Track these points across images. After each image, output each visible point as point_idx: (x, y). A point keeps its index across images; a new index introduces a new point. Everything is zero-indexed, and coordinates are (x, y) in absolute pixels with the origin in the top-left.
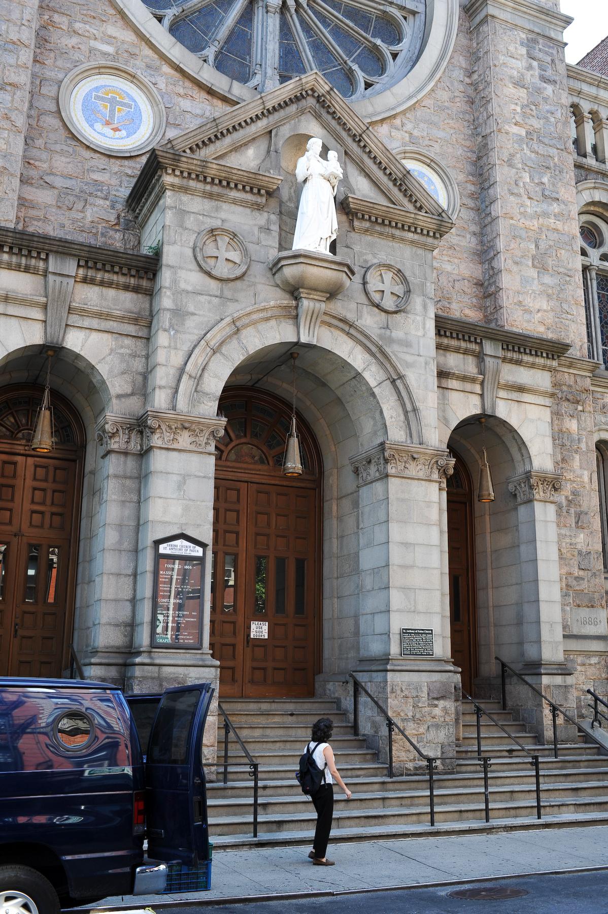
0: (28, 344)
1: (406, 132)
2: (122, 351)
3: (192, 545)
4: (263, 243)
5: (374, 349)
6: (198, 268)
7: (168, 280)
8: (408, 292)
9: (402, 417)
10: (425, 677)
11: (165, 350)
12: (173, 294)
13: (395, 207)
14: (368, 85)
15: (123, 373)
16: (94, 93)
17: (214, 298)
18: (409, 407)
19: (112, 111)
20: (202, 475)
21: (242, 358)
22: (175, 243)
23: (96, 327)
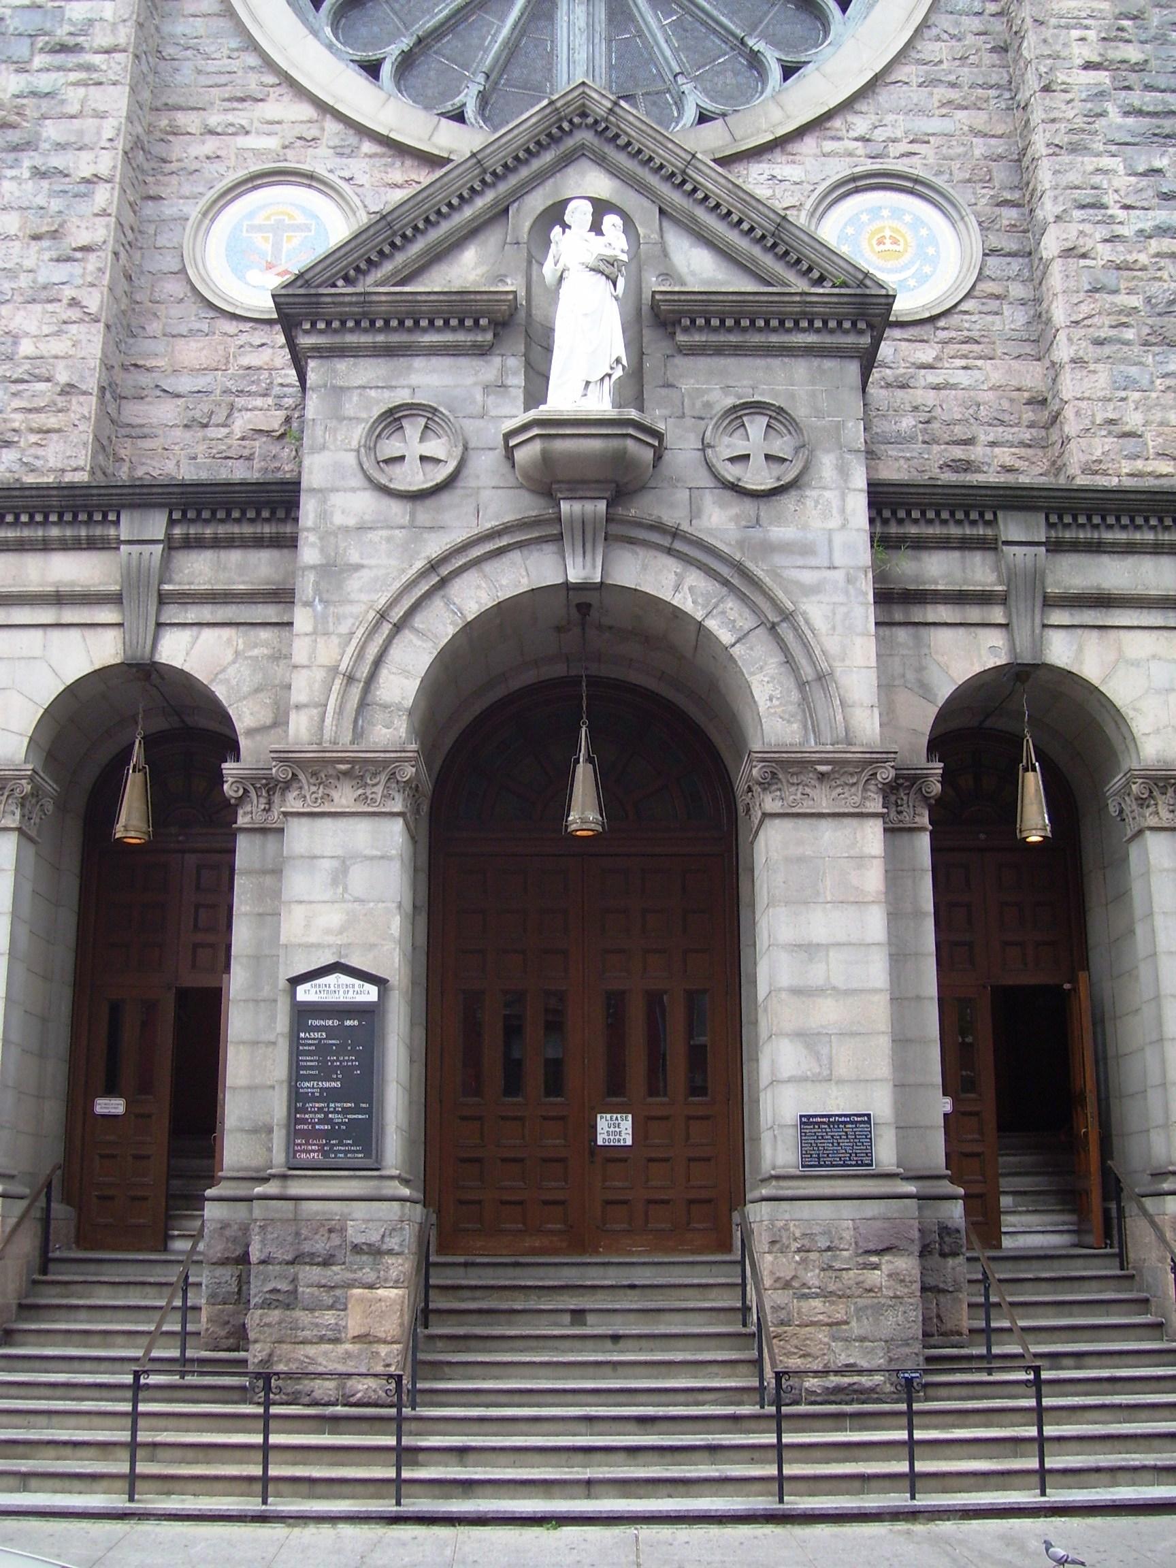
0: (97, 667)
1: (856, 139)
3: (357, 982)
4: (493, 413)
5: (725, 571)
6: (366, 484)
7: (311, 516)
10: (848, 1210)
11: (307, 639)
12: (321, 539)
13: (771, 289)
14: (789, 71)
17: (397, 532)
19: (277, 247)
20: (379, 853)
21: (451, 631)
22: (324, 447)
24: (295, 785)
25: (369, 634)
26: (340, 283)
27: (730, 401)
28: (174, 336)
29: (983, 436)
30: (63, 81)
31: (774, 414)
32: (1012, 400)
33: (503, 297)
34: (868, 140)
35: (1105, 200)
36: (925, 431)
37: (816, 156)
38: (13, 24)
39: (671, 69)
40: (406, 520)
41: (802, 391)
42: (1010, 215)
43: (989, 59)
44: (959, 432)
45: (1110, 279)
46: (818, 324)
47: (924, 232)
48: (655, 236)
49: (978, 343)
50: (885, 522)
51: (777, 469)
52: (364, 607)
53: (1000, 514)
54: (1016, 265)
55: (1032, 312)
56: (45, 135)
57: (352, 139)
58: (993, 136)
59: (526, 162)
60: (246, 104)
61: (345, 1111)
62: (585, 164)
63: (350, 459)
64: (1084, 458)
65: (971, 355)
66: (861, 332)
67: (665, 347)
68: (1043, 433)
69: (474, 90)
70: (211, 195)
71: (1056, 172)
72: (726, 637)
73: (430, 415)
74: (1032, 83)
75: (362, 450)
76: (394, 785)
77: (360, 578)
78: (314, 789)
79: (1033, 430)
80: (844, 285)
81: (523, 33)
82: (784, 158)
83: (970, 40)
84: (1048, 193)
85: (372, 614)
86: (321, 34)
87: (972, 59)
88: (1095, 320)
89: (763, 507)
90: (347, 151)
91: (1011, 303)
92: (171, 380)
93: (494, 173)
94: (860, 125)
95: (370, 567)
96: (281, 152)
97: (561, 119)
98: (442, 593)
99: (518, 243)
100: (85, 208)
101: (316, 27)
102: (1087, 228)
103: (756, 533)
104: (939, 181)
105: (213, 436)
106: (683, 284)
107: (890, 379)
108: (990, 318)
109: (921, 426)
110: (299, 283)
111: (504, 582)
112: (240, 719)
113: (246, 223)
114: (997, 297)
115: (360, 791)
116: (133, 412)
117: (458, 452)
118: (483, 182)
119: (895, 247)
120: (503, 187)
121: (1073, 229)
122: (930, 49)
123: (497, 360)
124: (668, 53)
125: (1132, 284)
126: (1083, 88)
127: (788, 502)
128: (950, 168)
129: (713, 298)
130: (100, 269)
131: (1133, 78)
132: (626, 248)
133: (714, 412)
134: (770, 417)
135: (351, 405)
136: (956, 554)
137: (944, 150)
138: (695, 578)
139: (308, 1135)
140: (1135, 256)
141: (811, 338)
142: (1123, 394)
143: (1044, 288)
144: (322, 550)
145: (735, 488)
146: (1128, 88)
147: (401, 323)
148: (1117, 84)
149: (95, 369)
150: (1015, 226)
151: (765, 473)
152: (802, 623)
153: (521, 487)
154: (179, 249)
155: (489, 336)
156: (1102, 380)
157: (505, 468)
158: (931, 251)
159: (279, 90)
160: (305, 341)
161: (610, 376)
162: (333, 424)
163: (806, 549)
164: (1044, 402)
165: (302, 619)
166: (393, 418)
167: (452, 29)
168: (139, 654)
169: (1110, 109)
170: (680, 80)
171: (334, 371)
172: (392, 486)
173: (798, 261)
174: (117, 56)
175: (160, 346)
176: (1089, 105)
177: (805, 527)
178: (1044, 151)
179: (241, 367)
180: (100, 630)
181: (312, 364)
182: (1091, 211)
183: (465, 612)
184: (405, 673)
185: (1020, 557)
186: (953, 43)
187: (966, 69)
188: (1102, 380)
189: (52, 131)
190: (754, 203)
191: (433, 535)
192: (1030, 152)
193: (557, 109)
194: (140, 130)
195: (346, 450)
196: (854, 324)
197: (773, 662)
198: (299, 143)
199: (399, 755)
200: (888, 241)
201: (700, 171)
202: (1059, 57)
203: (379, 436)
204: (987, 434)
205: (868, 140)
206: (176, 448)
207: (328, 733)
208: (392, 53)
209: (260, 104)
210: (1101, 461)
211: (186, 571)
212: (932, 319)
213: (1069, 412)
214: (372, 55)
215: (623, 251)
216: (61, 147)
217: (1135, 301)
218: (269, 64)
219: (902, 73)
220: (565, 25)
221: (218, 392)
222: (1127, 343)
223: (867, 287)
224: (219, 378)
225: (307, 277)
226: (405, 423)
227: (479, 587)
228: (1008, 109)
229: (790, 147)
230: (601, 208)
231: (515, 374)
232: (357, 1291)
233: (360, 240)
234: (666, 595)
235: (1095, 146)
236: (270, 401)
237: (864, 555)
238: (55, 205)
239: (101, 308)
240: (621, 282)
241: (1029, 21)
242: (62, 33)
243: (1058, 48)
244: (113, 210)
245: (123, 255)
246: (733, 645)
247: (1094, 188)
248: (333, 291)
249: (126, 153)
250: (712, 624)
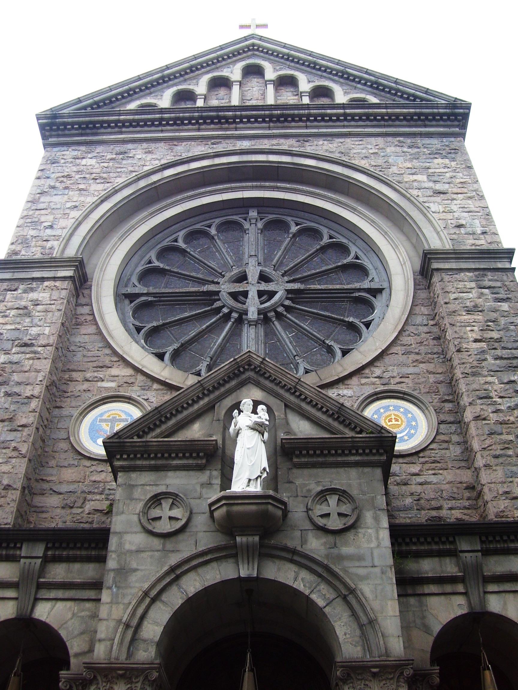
1: (376, 377)
2: (83, 614)
5: (319, 570)
6: (142, 530)
9: (358, 632)
11: (107, 606)
12: (118, 556)
14: (345, 353)
16: (99, 418)
17: (156, 553)
18: (364, 619)
21: (180, 602)
22: (123, 513)
24: (95, 682)
25: (139, 603)
26: (135, 437)
27: (319, 488)
28: (61, 467)
29: (446, 505)
30: (24, 357)
31: (341, 494)
32: (458, 488)
33: (211, 443)
34: (381, 378)
35: (491, 395)
36: (417, 504)
37: (358, 385)
38: (5, 336)
39: (292, 354)
40: (160, 547)
41: (355, 483)
42: (448, 406)
43: (432, 342)
44: (434, 504)
45: (498, 428)
46: (360, 451)
47: (410, 415)
48: (283, 416)
49: (439, 462)
50: (400, 544)
51: (344, 520)
52: (137, 590)
53: (457, 538)
54: (453, 427)
55: (463, 448)
56: (13, 379)
57: (149, 383)
58: (438, 373)
59: (223, 385)
60: (103, 369)
62: (250, 386)
63: (135, 518)
64: (495, 510)
65: (436, 468)
66: (381, 455)
67: (288, 464)
68: (475, 502)
69: (205, 364)
70: (84, 406)
71: (467, 384)
72: (321, 603)
73: (175, 498)
74: (452, 349)
75: (141, 514)
76: (147, 683)
77: (136, 575)
78: (104, 684)
79: (469, 501)
80: (372, 433)
81: (228, 341)
82: (344, 387)
83: (423, 335)
84: (465, 394)
85: (141, 593)
86: (139, 343)
87: (425, 343)
88: (493, 447)
89: (338, 538)
90: (147, 388)
91: (453, 444)
92: (58, 486)
93: (208, 390)
94: (378, 372)
95: (142, 570)
96: (117, 388)
97: (239, 367)
98: (176, 583)
99: (219, 420)
100: (25, 408)
101: (137, 340)
102: (484, 407)
103: (335, 551)
104: (415, 393)
105: (75, 512)
106: (295, 435)
107: (399, 481)
108: (443, 451)
109: (415, 502)
110: (116, 437)
111: (208, 577)
112: (72, 648)
113: (99, 418)
114: (447, 442)
115: (129, 686)
116: (38, 501)
117: (187, 514)
118: (203, 394)
119: (397, 423)
120: (212, 396)
121: (478, 408)
122: (405, 340)
123: (208, 473)
124: (291, 347)
125: (508, 430)
126: (475, 350)
127: (350, 535)
128: (419, 387)
129: (310, 441)
130: (29, 435)
131: (496, 345)
132: (268, 418)
133: (312, 494)
134: (340, 495)
135: (138, 493)
136: (436, 559)
137: (416, 380)
138: (304, 574)
140: (508, 418)
141: (358, 458)
142: (511, 480)
143: (468, 436)
144: (118, 562)
145: (324, 530)
146: (495, 349)
147: (163, 455)
148: (490, 347)
149: (21, 478)
150: (451, 410)
151: (338, 522)
152: (360, 594)
153: (218, 531)
154: (67, 429)
155: (204, 461)
156: (500, 474)
157: (210, 522)
158: (414, 423)
159: (118, 363)
160: (117, 463)
161: (261, 477)
162: (128, 502)
163: (360, 558)
164: (473, 488)
165: (105, 596)
167: (196, 341)
168: (24, 613)
169: (488, 357)
170: (297, 358)
171: (130, 477)
172: (154, 530)
173: (350, 424)
174: (48, 348)
175: (54, 471)
176: (478, 356)
177: (359, 547)
178: (461, 376)
179: (91, 481)
180: (6, 601)
181: (120, 474)
182: (485, 400)
183: (188, 593)
184: (157, 624)
185: (469, 559)
186: (416, 337)
187: (423, 347)
188: (500, 474)
189: (16, 377)
190: (328, 399)
191: (173, 554)
192: (455, 377)
193: (237, 362)
194: (55, 378)
195: (134, 514)
196: (378, 451)
197: (346, 615)
198: (125, 385)
199: (150, 666)
200: (393, 420)
201: (302, 386)
202: (463, 338)
203: (149, 508)
204: (447, 504)
205: (381, 378)
206: (57, 517)
207: (114, 654)
208: (170, 349)
209: (110, 369)
210: (504, 511)
211: (52, 573)
212: (417, 453)
213: (486, 490)
214: (161, 351)
215: (266, 420)
216: (19, 384)
217: (511, 437)
218: (115, 352)
219: (394, 350)
220: (246, 337)
221: (79, 492)
222: (510, 456)
223: (382, 433)
224: (80, 486)
225: (120, 434)
226: (163, 501)
227: (195, 580)
228: (443, 362)
229: (346, 382)
230: (256, 404)
231: (216, 478)
233: (145, 418)
234: (290, 582)
235: (484, 373)
236: (103, 496)
237: (390, 561)
238: (12, 408)
239: (27, 452)
240: (266, 435)
241: (448, 325)
242: (26, 339)
243: (462, 334)
244: (38, 410)
245: (41, 430)
246: (325, 607)
247: (485, 390)
248: (131, 440)
249: (47, 386)
250: (314, 597)
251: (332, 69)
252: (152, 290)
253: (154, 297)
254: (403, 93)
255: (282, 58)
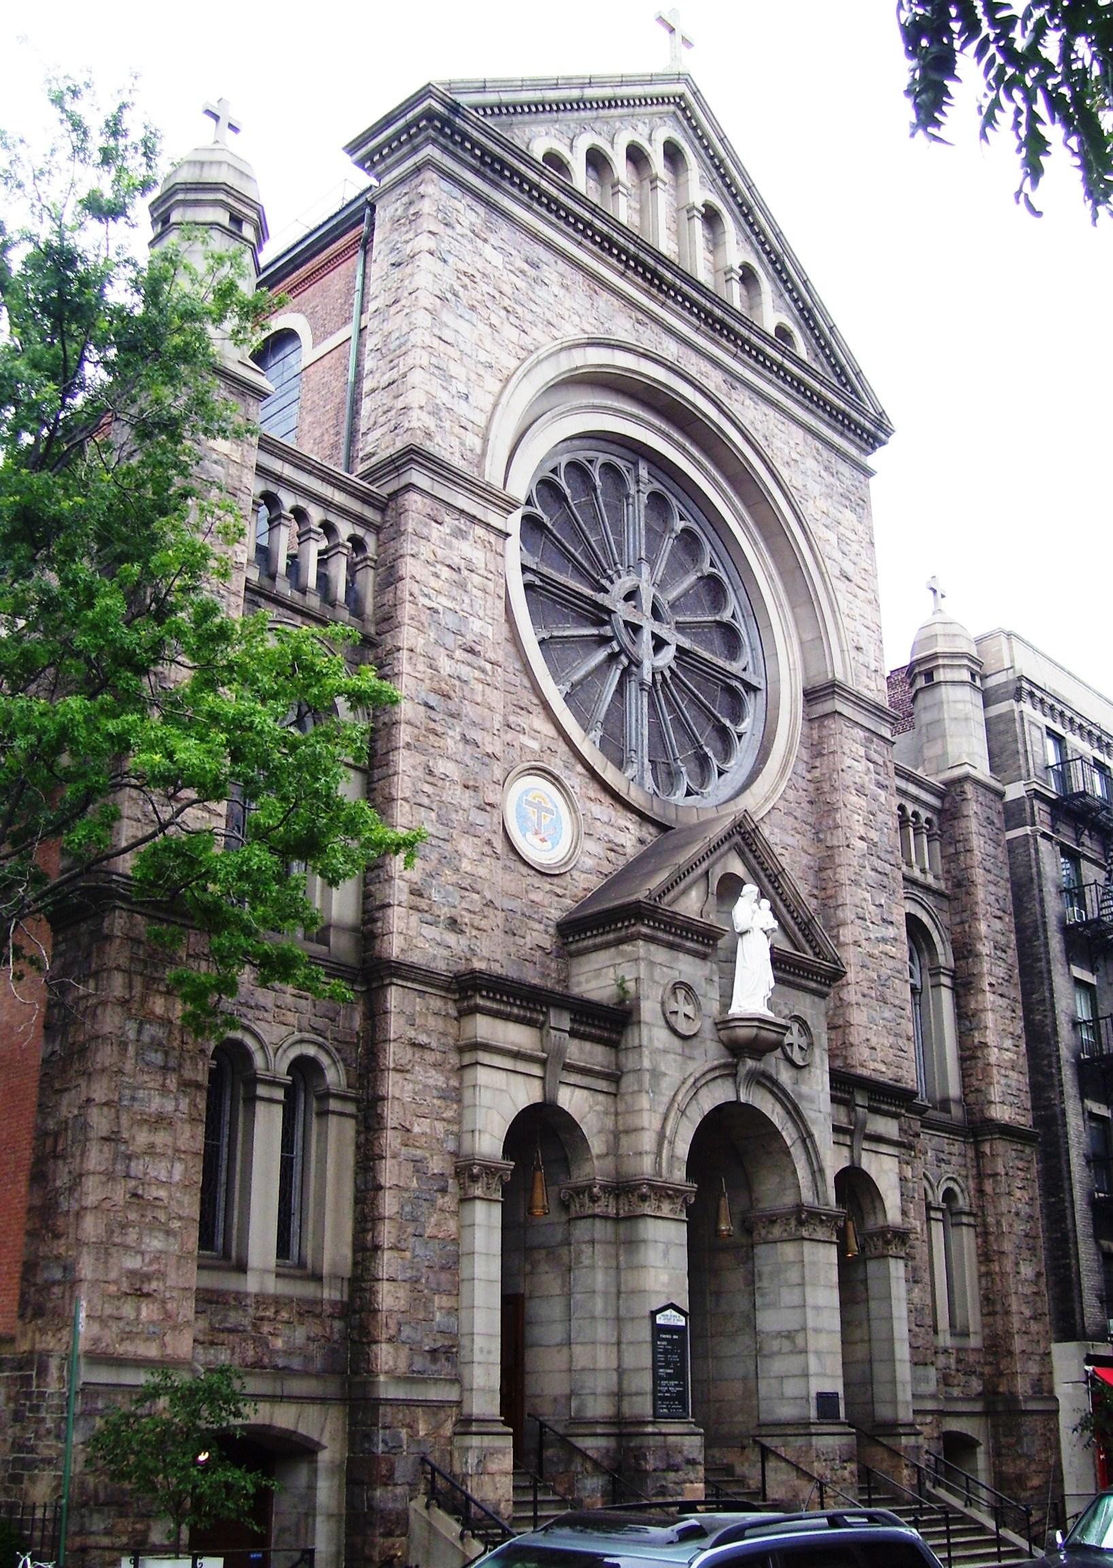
5: (790, 1106)
8: (811, 1044)
15: (600, 1132)
23: (579, 1083)
61: (676, 1386)
139: (663, 1399)
166: (679, 985)
177: (811, 1088)
232: (688, 1485)
251: (767, 241)
252: (546, 570)
253: (541, 580)
254: (833, 353)
255: (712, 158)
